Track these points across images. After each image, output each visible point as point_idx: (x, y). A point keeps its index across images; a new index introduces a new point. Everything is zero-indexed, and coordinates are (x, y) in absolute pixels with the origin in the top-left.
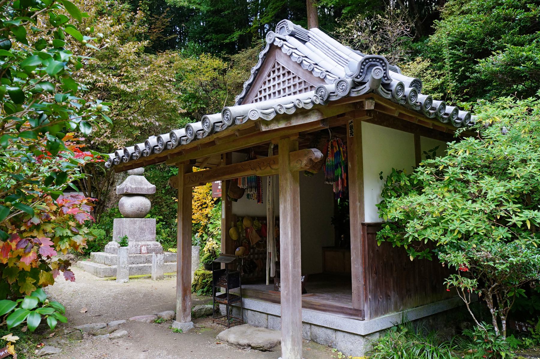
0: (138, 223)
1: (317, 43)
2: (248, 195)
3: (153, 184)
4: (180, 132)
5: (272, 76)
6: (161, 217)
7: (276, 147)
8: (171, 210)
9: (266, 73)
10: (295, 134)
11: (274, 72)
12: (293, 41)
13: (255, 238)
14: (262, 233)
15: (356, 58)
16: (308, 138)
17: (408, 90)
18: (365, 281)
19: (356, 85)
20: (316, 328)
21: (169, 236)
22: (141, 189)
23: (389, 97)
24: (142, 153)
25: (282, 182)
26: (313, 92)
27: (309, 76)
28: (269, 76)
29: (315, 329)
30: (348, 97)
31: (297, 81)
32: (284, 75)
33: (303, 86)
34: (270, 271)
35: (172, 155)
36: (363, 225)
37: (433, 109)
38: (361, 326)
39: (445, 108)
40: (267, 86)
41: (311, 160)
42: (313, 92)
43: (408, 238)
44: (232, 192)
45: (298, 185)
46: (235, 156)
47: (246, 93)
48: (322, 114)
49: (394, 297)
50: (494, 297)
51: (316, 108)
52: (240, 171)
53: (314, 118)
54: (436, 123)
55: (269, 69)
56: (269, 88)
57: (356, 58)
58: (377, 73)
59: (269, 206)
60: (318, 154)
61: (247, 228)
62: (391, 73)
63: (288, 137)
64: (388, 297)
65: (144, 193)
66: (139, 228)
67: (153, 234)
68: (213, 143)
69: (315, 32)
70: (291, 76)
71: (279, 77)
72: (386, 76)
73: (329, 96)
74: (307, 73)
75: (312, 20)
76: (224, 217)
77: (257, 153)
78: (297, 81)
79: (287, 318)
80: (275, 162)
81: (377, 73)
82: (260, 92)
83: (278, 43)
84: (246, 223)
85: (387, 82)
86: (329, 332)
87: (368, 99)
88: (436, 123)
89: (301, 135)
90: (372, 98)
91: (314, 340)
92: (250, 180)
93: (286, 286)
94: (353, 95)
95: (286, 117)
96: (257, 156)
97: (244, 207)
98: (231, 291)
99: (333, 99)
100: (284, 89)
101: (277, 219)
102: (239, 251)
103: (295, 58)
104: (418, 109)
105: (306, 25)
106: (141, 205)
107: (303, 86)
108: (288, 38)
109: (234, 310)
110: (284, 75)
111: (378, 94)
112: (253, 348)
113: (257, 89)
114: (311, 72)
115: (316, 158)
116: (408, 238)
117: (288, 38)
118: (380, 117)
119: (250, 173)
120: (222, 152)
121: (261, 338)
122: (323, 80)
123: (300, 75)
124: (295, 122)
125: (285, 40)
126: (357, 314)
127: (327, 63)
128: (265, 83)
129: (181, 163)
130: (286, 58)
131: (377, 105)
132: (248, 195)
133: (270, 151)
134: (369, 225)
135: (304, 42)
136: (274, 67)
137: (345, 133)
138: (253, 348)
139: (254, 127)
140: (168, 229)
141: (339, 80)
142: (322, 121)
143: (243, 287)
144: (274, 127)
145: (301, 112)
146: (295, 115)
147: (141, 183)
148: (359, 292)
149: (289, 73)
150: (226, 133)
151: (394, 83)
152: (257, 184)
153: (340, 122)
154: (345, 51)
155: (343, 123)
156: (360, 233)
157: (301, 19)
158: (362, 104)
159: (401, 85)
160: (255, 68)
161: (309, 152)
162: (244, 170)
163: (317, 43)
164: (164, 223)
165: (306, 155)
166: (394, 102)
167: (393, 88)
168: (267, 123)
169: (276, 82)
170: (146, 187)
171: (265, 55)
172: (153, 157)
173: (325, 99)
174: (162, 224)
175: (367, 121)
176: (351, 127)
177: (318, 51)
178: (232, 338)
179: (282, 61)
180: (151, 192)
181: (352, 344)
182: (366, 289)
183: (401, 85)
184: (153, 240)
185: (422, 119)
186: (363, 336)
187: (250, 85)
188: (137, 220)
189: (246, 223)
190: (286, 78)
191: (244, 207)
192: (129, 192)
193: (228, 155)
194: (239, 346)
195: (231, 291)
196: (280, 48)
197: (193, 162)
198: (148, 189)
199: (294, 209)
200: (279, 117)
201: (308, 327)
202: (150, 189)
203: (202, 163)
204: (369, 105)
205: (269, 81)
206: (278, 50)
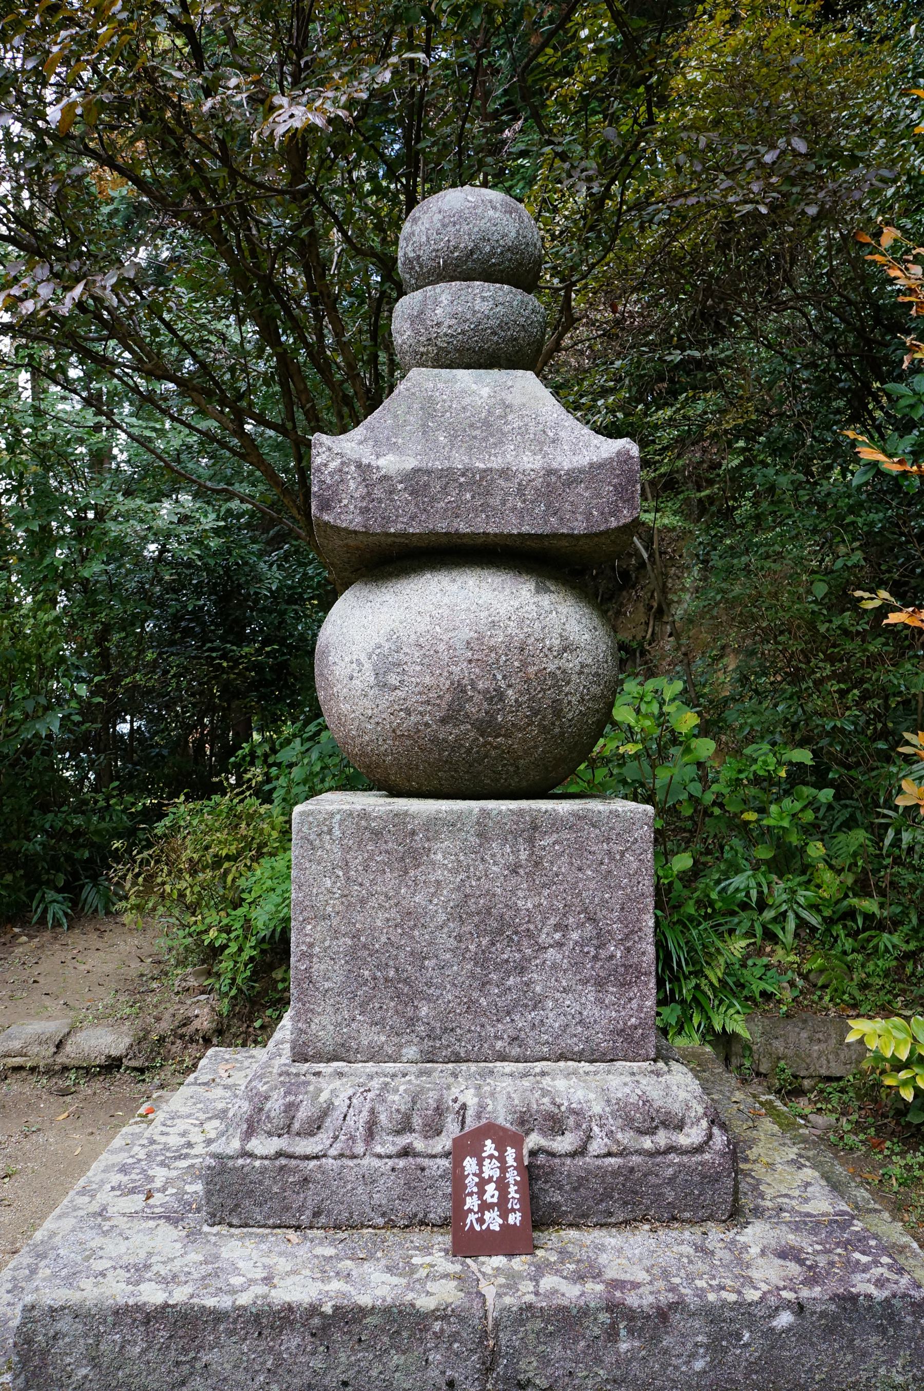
0: (443, 853)
3: (611, 431)
6: (804, 756)
8: (875, 704)
21: (862, 888)
22: (481, 482)
43: (907, 743)
65: (513, 526)
66: (459, 913)
67: (625, 974)
106: (480, 651)
116: (907, 743)
140: (860, 836)
147: (489, 427)
164: (826, 795)
170: (530, 462)
174: (812, 804)
180: (578, 518)
184: (619, 1047)
188: (432, 825)
198: (557, 484)
202: (573, 478)
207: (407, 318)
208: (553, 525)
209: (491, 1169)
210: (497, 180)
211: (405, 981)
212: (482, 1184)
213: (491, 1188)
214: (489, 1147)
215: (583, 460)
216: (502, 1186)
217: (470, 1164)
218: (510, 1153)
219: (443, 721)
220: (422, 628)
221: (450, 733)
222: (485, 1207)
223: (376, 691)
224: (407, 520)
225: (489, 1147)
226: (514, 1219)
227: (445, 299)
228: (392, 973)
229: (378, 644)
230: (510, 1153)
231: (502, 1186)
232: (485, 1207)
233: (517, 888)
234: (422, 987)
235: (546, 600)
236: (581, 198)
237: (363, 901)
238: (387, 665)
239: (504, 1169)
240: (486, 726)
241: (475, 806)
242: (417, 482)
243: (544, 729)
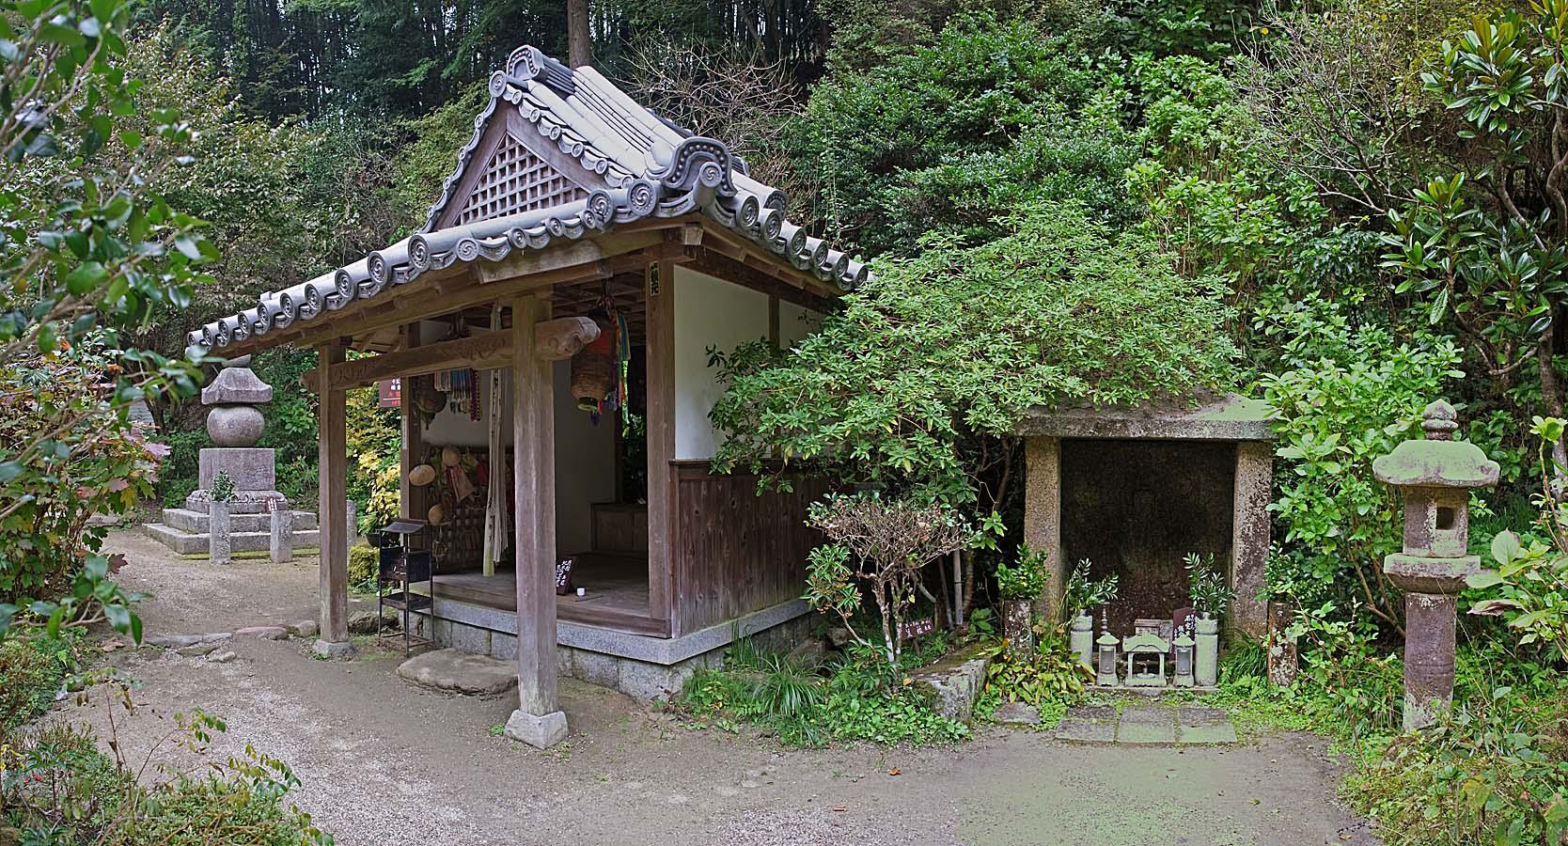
1: (590, 100)
2: (453, 405)
4: (325, 282)
5: (498, 166)
7: (507, 311)
9: (487, 160)
10: (546, 288)
11: (502, 156)
12: (543, 93)
13: (464, 488)
14: (479, 477)
15: (668, 140)
16: (569, 298)
17: (764, 213)
18: (674, 568)
19: (669, 193)
20: (582, 655)
23: (730, 223)
24: (253, 328)
25: (520, 382)
26: (584, 202)
27: (573, 169)
28: (493, 164)
29: (580, 657)
30: (652, 218)
31: (549, 176)
32: (523, 163)
33: (561, 188)
34: (492, 551)
35: (309, 331)
36: (672, 464)
37: (807, 252)
38: (663, 650)
39: (847, 264)
40: (488, 185)
41: (577, 339)
42: (584, 202)
44: (423, 400)
45: (551, 388)
46: (426, 330)
47: (449, 201)
48: (601, 249)
49: (723, 594)
50: (887, 586)
51: (590, 236)
52: (440, 359)
53: (585, 257)
54: (810, 280)
55: (493, 149)
56: (493, 190)
57: (668, 140)
58: (708, 175)
59: (493, 426)
60: (590, 328)
61: (449, 468)
62: (736, 177)
63: (531, 292)
64: (712, 595)
68: (390, 306)
69: (587, 75)
70: (537, 167)
71: (512, 167)
72: (726, 182)
73: (615, 213)
74: (546, 145)
75: (576, 48)
76: (405, 447)
77: (470, 321)
78: (549, 176)
79: (529, 639)
80: (506, 342)
81: (708, 175)
82: (475, 197)
83: (512, 95)
84: (449, 458)
85: (726, 194)
86: (605, 660)
87: (689, 224)
88: (810, 280)
89: (557, 288)
90: (697, 223)
91: (577, 675)
92: (455, 375)
93: (526, 581)
94: (662, 214)
95: (531, 254)
96: (472, 328)
97: (447, 427)
98: (415, 588)
99: (623, 220)
100: (523, 193)
101: (510, 450)
102: (434, 514)
103: (590, 162)
104: (781, 250)
105: (564, 56)
107: (561, 188)
108: (531, 85)
109: (426, 623)
110: (523, 163)
111: (709, 215)
112: (466, 693)
113: (468, 191)
114: (578, 160)
115: (588, 337)
117: (531, 85)
118: (712, 260)
119: (460, 363)
120: (404, 322)
121: (481, 674)
122: (601, 178)
123: (556, 163)
124: (545, 265)
125: (525, 90)
126: (659, 628)
127: (609, 143)
128: (484, 180)
129: (324, 344)
130: (528, 129)
131: (706, 237)
132: (453, 405)
133: (495, 318)
134: (683, 465)
135: (564, 96)
136: (503, 145)
137: (641, 285)
138: (466, 693)
139: (465, 275)
141: (632, 181)
142: (602, 262)
143: (435, 579)
144: (507, 274)
145: (560, 244)
146: (549, 249)
147: (244, 381)
148: (662, 588)
149: (533, 159)
150: (416, 287)
151: (741, 198)
152: (470, 383)
153: (634, 265)
154: (643, 117)
155: (639, 266)
156: (666, 480)
157: (554, 45)
158: (677, 234)
159: (752, 201)
160: (467, 148)
161: (573, 323)
162: (451, 358)
163: (590, 100)
165: (567, 330)
166: (737, 233)
167: (738, 208)
168: (493, 267)
169: (506, 179)
171: (486, 120)
172: (274, 335)
173: (607, 218)
175: (685, 265)
176: (654, 277)
177: (591, 115)
178: (425, 674)
179: (520, 136)
181: (648, 681)
182: (675, 584)
183: (752, 201)
185: (786, 270)
186: (669, 667)
187: (457, 184)
189: (449, 458)
190: (527, 170)
191: (447, 427)
192: (225, 398)
193: (414, 327)
194: (437, 688)
195: (415, 588)
196: (516, 107)
197: (346, 342)
199: (542, 436)
200: (516, 255)
201: (567, 653)
203: (361, 341)
204: (692, 237)
205: (493, 175)
206: (512, 111)
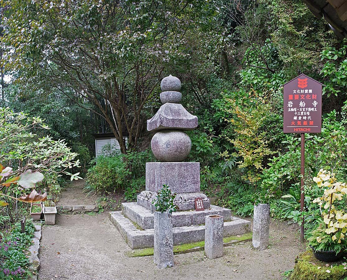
147: (178, 113)
202: (190, 121)
207: (163, 95)
208: (188, 127)
209: (199, 202)
210: (180, 78)
211: (173, 184)
212: (199, 204)
213: (199, 204)
214: (199, 200)
215: (191, 118)
216: (201, 204)
217: (197, 202)
218: (201, 200)
219: (175, 152)
220: (173, 140)
221: (176, 153)
222: (199, 206)
223: (166, 148)
224: (171, 126)
225: (199, 200)
226: (202, 207)
227: (171, 93)
228: (171, 183)
229: (162, 141)
230: (201, 200)
231: (201, 204)
232: (199, 206)
233: (185, 172)
234: (174, 185)
235: (186, 136)
236: (33, 22)
237: (168, 174)
238: (168, 144)
239: (200, 202)
240: (180, 153)
241: (180, 162)
242: (173, 120)
243: (186, 153)
